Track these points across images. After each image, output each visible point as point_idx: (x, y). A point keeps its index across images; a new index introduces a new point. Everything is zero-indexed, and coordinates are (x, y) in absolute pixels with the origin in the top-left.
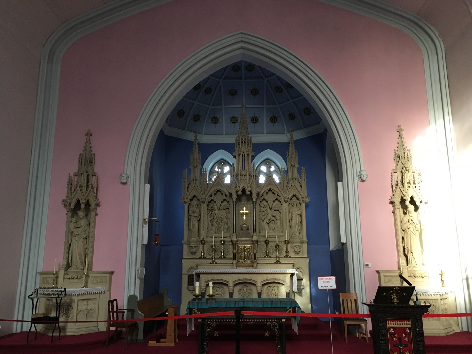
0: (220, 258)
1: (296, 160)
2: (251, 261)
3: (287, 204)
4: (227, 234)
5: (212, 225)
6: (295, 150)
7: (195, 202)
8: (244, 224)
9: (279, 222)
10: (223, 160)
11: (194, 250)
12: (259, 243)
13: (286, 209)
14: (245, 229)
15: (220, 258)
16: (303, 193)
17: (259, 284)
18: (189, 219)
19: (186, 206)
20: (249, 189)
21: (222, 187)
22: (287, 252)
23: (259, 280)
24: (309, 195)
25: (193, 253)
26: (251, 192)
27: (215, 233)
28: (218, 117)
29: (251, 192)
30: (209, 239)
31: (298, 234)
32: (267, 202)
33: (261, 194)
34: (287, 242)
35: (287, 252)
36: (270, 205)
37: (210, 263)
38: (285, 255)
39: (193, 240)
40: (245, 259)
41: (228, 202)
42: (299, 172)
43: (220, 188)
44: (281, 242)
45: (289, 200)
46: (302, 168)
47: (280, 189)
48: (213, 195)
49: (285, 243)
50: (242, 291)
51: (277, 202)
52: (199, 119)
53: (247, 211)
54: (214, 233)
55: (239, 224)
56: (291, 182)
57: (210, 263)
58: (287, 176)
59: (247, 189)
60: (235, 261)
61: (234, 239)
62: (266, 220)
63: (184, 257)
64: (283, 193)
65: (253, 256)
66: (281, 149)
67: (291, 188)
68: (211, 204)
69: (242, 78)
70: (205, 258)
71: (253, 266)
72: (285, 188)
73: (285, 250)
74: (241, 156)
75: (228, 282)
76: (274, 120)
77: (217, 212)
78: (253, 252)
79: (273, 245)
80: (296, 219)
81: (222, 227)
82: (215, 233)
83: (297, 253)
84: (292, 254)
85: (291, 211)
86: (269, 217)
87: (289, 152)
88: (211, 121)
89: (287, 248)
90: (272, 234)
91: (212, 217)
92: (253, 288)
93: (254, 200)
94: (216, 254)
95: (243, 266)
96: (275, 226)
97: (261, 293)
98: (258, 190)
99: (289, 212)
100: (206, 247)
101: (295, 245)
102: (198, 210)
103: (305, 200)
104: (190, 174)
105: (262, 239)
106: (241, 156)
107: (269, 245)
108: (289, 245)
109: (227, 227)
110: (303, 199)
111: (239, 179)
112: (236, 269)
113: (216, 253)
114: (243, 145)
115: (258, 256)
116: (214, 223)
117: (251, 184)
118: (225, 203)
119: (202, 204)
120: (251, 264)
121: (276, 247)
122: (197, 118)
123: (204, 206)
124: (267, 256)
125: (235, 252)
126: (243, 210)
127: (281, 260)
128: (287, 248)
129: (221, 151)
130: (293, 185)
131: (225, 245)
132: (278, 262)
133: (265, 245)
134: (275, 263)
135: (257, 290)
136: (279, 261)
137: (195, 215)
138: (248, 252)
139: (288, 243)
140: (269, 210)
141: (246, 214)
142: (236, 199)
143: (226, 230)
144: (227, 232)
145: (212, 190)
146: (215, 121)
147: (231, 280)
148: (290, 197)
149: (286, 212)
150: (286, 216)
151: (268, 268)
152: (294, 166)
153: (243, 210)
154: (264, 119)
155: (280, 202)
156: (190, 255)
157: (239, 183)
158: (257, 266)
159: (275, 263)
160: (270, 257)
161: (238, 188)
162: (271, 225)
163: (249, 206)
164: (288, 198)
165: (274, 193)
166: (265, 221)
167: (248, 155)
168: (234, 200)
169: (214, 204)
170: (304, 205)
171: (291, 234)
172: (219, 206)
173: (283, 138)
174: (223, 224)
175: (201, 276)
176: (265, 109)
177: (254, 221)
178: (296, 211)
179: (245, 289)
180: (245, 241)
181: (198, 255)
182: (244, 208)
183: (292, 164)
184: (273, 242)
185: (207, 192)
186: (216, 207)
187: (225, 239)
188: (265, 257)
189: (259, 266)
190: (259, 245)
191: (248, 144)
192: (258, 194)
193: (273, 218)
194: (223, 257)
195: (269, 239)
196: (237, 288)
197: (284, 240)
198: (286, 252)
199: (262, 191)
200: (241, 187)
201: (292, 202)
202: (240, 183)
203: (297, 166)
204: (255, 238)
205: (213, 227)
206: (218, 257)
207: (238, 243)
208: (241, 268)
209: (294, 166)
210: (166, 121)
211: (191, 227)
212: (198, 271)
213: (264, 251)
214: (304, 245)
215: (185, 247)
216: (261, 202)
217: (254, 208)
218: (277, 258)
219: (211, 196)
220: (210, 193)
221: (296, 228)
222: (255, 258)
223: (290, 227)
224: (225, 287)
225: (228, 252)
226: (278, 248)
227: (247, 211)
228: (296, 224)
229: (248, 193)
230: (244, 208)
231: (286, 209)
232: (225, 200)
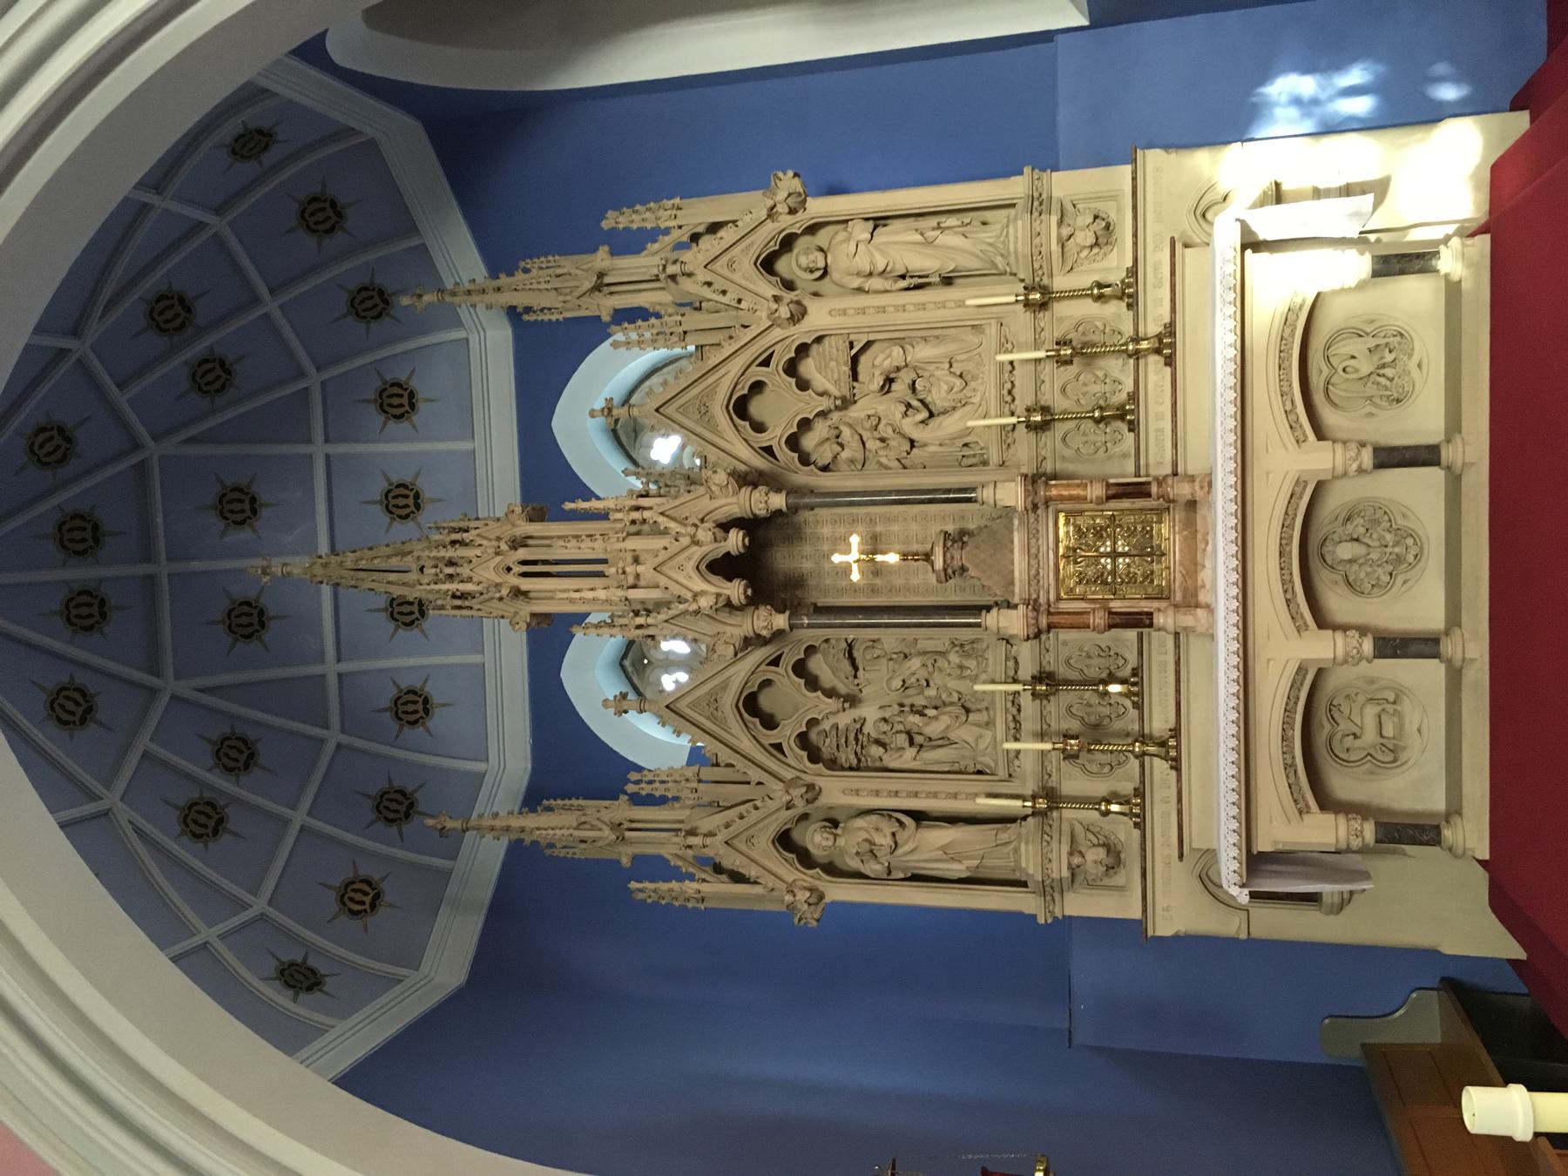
0: (1138, 706)
1: (567, 264)
2: (1160, 512)
3: (813, 306)
4: (996, 657)
5: (945, 741)
6: (519, 276)
7: (816, 840)
8: (927, 557)
9: (922, 352)
10: (624, 656)
11: (1095, 855)
12: (1048, 467)
13: (844, 312)
14: (960, 556)
15: (1138, 706)
16: (751, 213)
17: (1319, 459)
18: (916, 878)
19: (841, 892)
20: (704, 534)
21: (724, 686)
22: (1100, 292)
23: (1287, 460)
24: (762, 183)
25: (1115, 858)
26: (725, 527)
27: (989, 724)
28: (394, 692)
29: (725, 527)
30: (1028, 766)
31: (988, 235)
32: (805, 424)
33: (760, 462)
34: (1040, 299)
35: (1100, 292)
36: (825, 403)
37: (1176, 765)
38: (1116, 308)
39: (1029, 862)
40: (1148, 551)
41: (811, 650)
42: (630, 242)
43: (729, 699)
44: (1038, 331)
45: (788, 296)
46: (605, 225)
47: (728, 349)
48: (772, 737)
49: (1043, 306)
50: (1358, 573)
51: (808, 368)
52: (402, 792)
53: (855, 540)
54: (988, 735)
55: (924, 586)
56: (687, 285)
57: (1176, 765)
58: (658, 316)
59: (711, 545)
60: (1159, 619)
61: (1013, 622)
62: (909, 426)
63: (1138, 915)
64: (748, 335)
65: (1126, 504)
66: (548, 354)
67: (720, 284)
68: (827, 749)
69: (151, 579)
70: (1139, 792)
71: (1192, 505)
72: (720, 320)
73: (1087, 308)
74: (526, 584)
75: (1301, 670)
76: (397, 402)
77: (869, 712)
78: (1099, 501)
79: (1055, 377)
80: (902, 248)
81: (953, 684)
82: (989, 724)
83: (1105, 236)
84: (1113, 267)
85: (857, 282)
86: (890, 409)
87: (528, 310)
88: (420, 730)
89: (1075, 295)
90: (987, 388)
91: (902, 740)
92: (1337, 499)
93: (778, 501)
94: (1117, 725)
95: (1193, 565)
96: (942, 373)
97: (1377, 450)
98: (721, 477)
99: (860, 290)
100: (1073, 782)
101: (1055, 247)
102: (860, 822)
103: (782, 195)
104: (660, 859)
105: (1025, 449)
106: (526, 584)
107: (1060, 403)
108: (1060, 282)
109: (954, 658)
110: (783, 208)
111: (655, 594)
112: (1210, 609)
113: (1104, 713)
114: (465, 571)
115: (1125, 472)
116: (934, 729)
117: (683, 522)
118: (817, 664)
119: (823, 800)
120: (1179, 515)
121: (1068, 362)
122: (396, 807)
123: (836, 791)
124: (1124, 415)
125: (1099, 619)
126: (846, 569)
127: (1153, 328)
128: (1075, 295)
129: (567, 675)
130: (703, 276)
131: (1063, 672)
132: (1166, 346)
133: (1060, 429)
134: (1170, 361)
135: (1361, 471)
136: (1159, 337)
137: (884, 840)
138: (1099, 533)
139: (1045, 290)
140: (856, 412)
141: (874, 545)
142: (780, 611)
143: (972, 663)
144: (980, 656)
145: (746, 744)
146: (412, 707)
147: (1288, 649)
148: (770, 291)
149: (862, 311)
150: (882, 310)
151: (1203, 417)
152: (601, 275)
153: (846, 569)
154: (396, 450)
155: (803, 350)
156: (1119, 879)
157: (680, 600)
158: (1192, 479)
159: (1170, 361)
160: (1134, 397)
161: (704, 602)
162: (938, 398)
163: (826, 531)
164: (777, 299)
165: (758, 387)
166: (916, 434)
167: (516, 544)
168: (781, 621)
169: (826, 725)
170: (820, 207)
171: (989, 274)
172: (832, 704)
173: (493, 347)
174: (937, 679)
175: (1263, 845)
176: (342, 448)
177: (908, 497)
178: (852, 252)
179: (1345, 551)
180: (1032, 555)
181: (1124, 832)
182: (837, 558)
183: (588, 285)
184: (1038, 384)
185: (755, 774)
186: (844, 719)
187: (1026, 672)
188: (1133, 427)
189: (1192, 466)
190: (1060, 466)
191: (462, 543)
192: (747, 479)
193: (900, 387)
194: (1136, 680)
195: (1020, 406)
196: (1339, 604)
197: (1023, 317)
198: (1100, 298)
199: (744, 452)
200: (698, 584)
201: (803, 278)
202: (676, 590)
203: (602, 259)
204: (1012, 494)
205: (953, 736)
206: (1133, 713)
207: (1048, 594)
208: (1204, 576)
209: (601, 275)
210: (290, 1054)
211: (959, 869)
212: (1229, 867)
213: (1095, 434)
214: (1056, 194)
215: (1079, 905)
216: (805, 460)
217: (835, 499)
218: (1137, 355)
219: (778, 747)
220: (761, 757)
221: (955, 247)
222: (1137, 490)
223: (948, 281)
224: (1332, 683)
225: (1104, 652)
226: (1076, 352)
227: (855, 540)
228: (929, 243)
229: (735, 541)
230: (837, 558)
231: (844, 312)
232: (800, 669)
